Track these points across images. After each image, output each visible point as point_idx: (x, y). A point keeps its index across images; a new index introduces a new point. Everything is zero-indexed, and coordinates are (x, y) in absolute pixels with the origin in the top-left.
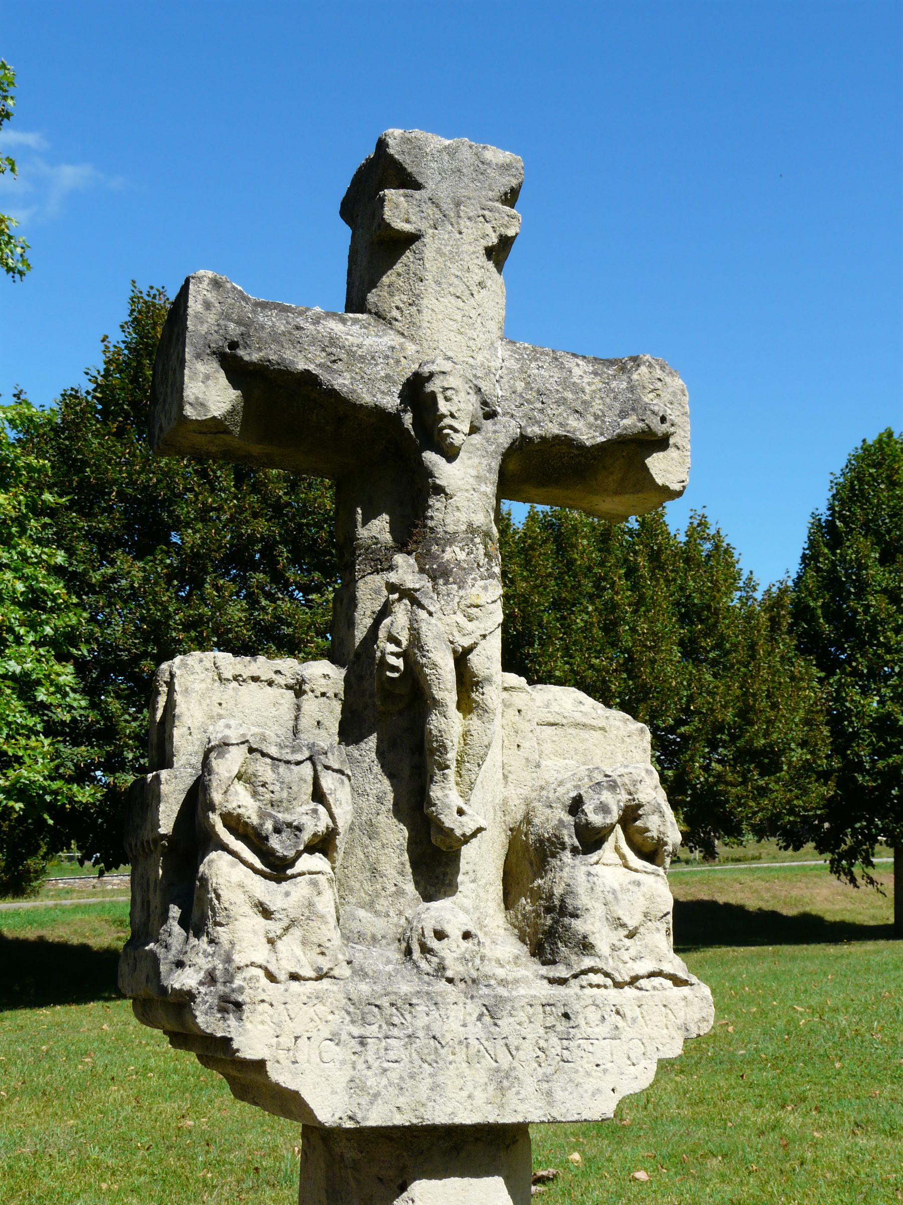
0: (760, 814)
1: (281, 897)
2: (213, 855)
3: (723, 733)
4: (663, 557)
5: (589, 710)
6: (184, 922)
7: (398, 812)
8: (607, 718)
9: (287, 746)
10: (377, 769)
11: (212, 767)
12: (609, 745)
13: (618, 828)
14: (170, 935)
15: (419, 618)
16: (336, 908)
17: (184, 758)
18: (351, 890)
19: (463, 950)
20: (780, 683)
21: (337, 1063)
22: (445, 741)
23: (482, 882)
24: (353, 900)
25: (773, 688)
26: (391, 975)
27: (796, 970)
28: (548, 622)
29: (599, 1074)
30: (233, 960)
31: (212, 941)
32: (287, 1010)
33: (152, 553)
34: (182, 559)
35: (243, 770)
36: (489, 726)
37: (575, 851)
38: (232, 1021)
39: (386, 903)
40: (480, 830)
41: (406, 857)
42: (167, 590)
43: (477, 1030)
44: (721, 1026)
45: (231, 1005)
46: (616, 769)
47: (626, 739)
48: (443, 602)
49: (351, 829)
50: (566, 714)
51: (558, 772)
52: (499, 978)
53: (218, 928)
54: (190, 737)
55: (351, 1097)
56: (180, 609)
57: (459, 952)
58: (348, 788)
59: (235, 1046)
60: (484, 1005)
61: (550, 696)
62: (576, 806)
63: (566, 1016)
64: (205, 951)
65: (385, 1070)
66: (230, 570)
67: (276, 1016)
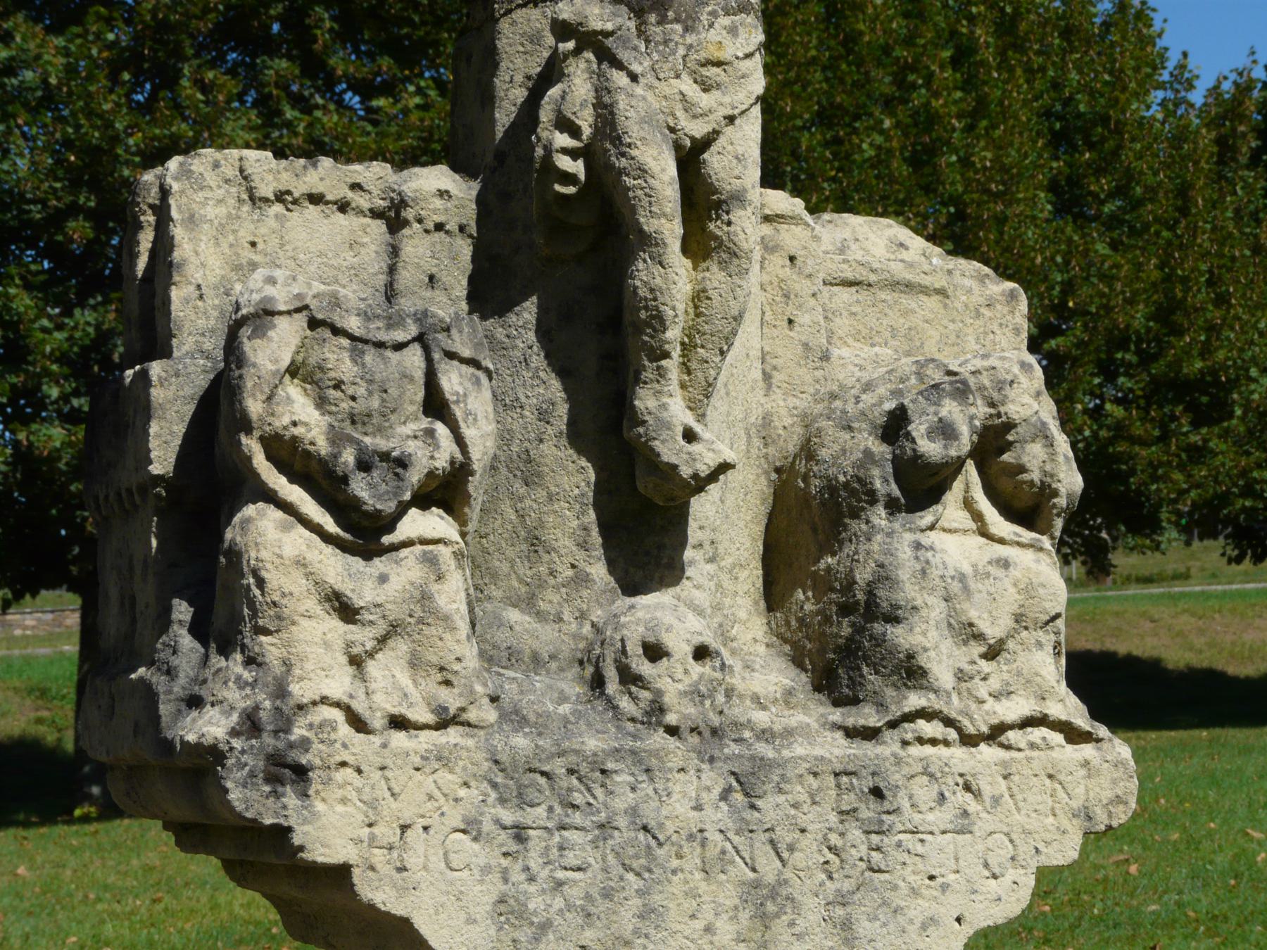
0: (1193, 494)
1: (381, 584)
2: (250, 510)
3: (1127, 350)
4: (1023, 26)
5: (917, 258)
6: (198, 629)
7: (577, 436)
8: (950, 272)
9: (378, 317)
10: (538, 360)
11: (243, 353)
12: (953, 321)
13: (970, 468)
14: (175, 653)
15: (612, 86)
16: (469, 604)
17: (191, 339)
18: (494, 576)
19: (695, 677)
20: (1233, 259)
21: (475, 871)
22: (662, 308)
23: (727, 562)
24: (497, 593)
25: (1220, 267)
27: (1250, 770)
28: (810, 149)
29: (935, 893)
30: (290, 694)
31: (250, 661)
33: (79, 21)
34: (135, 31)
35: (300, 358)
36: (739, 282)
37: (893, 507)
38: (291, 799)
39: (556, 598)
40: (724, 467)
41: (592, 516)
42: (111, 91)
43: (719, 815)
44: (1117, 863)
45: (289, 771)
46: (967, 361)
47: (983, 310)
48: (656, 56)
49: (493, 468)
50: (875, 265)
51: (862, 368)
53: (263, 638)
54: (200, 303)
55: (501, 929)
56: (136, 125)
57: (687, 681)
58: (487, 395)
60: (733, 773)
61: (847, 234)
62: (894, 426)
63: (877, 793)
64: (239, 678)
65: (560, 884)
66: (226, 53)
67: (367, 789)
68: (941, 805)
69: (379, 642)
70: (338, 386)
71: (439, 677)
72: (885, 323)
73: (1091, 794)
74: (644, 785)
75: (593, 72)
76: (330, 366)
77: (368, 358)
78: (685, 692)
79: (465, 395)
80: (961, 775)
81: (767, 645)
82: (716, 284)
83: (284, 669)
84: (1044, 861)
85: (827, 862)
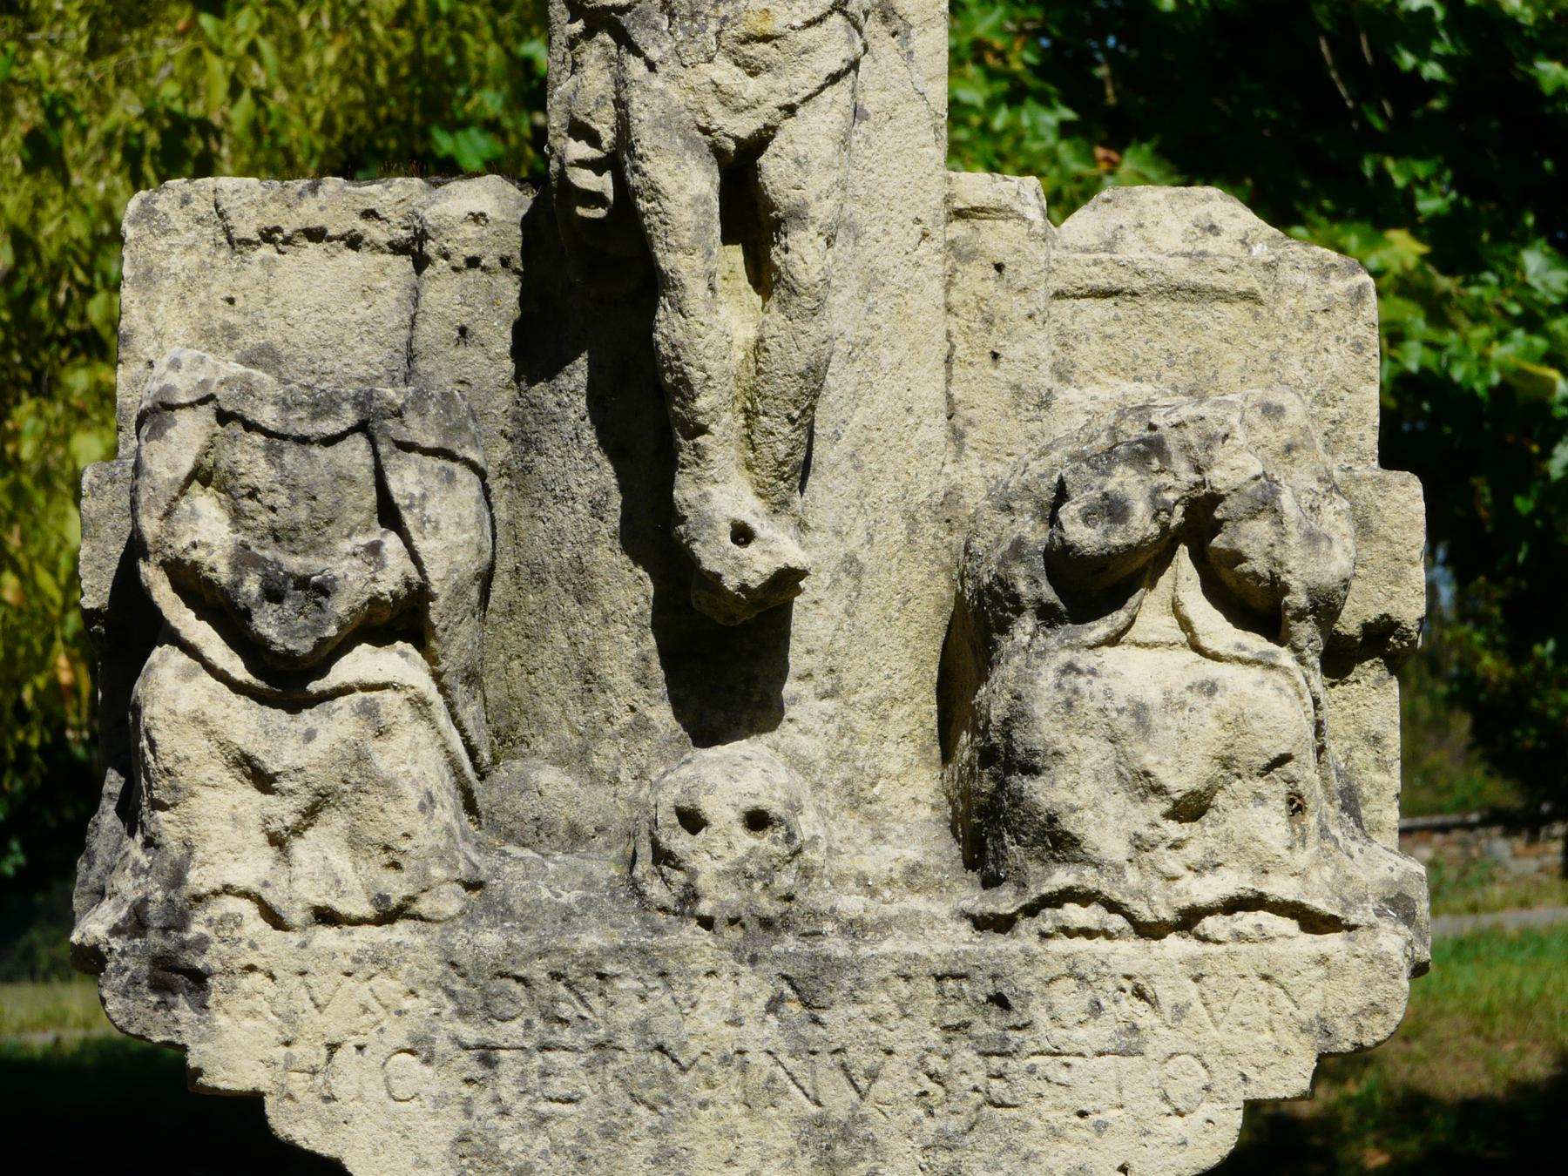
1: (301, 743)
9: (301, 404)
10: (589, 436)
12: (1267, 337)
19: (741, 852)
22: (687, 369)
24: (544, 747)
26: (573, 913)
29: (1086, 1135)
31: (149, 843)
32: (309, 987)
35: (209, 462)
37: (1048, 616)
38: (184, 1011)
39: (611, 751)
41: (651, 642)
43: (766, 1032)
48: (680, 35)
50: (1141, 266)
52: (846, 917)
53: (159, 814)
59: (192, 1062)
60: (785, 977)
63: (1000, 1001)
64: (136, 863)
65: (543, 1119)
67: (282, 999)
68: (1096, 1018)
69: (305, 816)
70: (253, 494)
71: (385, 858)
72: (1157, 346)
73: (1331, 1001)
74: (657, 993)
75: (612, 59)
76: (241, 470)
77: (288, 458)
78: (726, 873)
79: (424, 497)
80: (1128, 977)
81: (933, 808)
82: (774, 331)
83: (185, 851)
84: (1255, 1092)
85: (925, 1094)
